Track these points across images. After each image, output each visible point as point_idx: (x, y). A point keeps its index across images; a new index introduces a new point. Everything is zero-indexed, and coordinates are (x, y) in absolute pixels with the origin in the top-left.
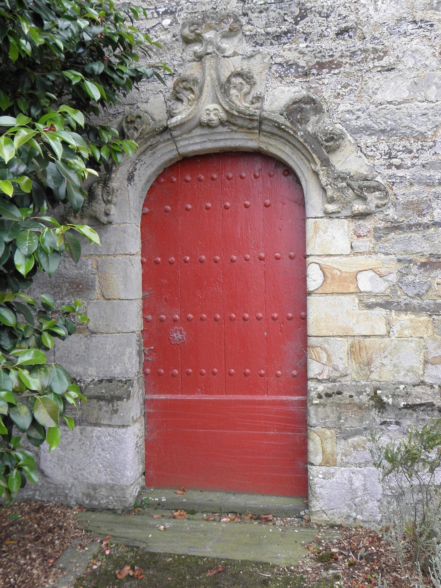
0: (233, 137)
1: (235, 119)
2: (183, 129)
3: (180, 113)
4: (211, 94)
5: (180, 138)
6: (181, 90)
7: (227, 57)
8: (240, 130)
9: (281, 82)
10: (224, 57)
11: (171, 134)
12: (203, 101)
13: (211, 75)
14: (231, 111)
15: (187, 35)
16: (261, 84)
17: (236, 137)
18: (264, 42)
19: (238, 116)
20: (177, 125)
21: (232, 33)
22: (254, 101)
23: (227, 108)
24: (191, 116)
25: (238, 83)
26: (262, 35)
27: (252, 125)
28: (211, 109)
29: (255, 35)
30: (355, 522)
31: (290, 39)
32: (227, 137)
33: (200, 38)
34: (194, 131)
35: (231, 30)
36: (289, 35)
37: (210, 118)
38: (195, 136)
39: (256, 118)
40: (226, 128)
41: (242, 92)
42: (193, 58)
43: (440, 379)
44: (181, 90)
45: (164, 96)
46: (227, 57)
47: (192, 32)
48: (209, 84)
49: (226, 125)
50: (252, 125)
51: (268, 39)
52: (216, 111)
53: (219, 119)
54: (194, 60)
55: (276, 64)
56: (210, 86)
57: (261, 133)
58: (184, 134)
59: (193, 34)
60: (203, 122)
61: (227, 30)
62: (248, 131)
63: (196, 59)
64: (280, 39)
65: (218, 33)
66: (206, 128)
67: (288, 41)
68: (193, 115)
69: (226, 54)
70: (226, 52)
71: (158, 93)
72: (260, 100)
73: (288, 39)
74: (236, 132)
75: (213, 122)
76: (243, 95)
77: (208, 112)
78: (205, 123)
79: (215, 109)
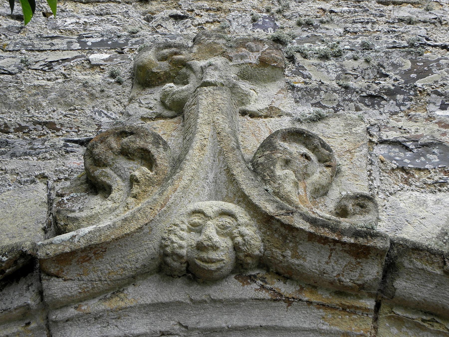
0: (277, 323)
1: (294, 249)
2: (93, 276)
3: (90, 219)
4: (211, 176)
5: (71, 312)
6: (110, 156)
7: (253, 115)
8: (306, 297)
9: (406, 182)
10: (244, 113)
11: (41, 293)
12: (183, 183)
13: (214, 124)
14: (286, 219)
15: (151, 62)
16: (355, 175)
17: (287, 324)
18: (339, 105)
19: (311, 237)
20: (73, 253)
21: (267, 71)
22: (350, 207)
23: (270, 208)
24: (133, 226)
25: (296, 155)
26: (335, 91)
27: (355, 275)
28: (209, 212)
29: (318, 90)
30: (27, 109)
31: (403, 105)
32: (255, 322)
33: (184, 70)
34: (131, 289)
35: (263, 63)
36: (400, 97)
37: (202, 238)
38: (131, 309)
39: (379, 244)
40: (255, 286)
41: (309, 181)
42: (159, 109)
43: (51, 336)
44: (110, 156)
45: (49, 189)
46: (253, 115)
47: (164, 58)
48: (209, 144)
49: (253, 279)
50: (355, 275)
51: (351, 100)
52: (227, 220)
53: (236, 248)
54: (159, 116)
55: (382, 142)
56: (208, 151)
57: (384, 310)
58: (93, 296)
59: (165, 64)
60: (174, 254)
61: (254, 61)
62: (336, 301)
63: (166, 113)
64: (379, 104)
65: (231, 64)
66: (179, 282)
67: (397, 109)
68: (142, 222)
69: (252, 107)
70: (249, 102)
71: (33, 182)
72: (370, 205)
73: (399, 105)
74: (289, 301)
75: (213, 255)
76: (310, 188)
77: (196, 219)
78: (180, 257)
79: (224, 213)
